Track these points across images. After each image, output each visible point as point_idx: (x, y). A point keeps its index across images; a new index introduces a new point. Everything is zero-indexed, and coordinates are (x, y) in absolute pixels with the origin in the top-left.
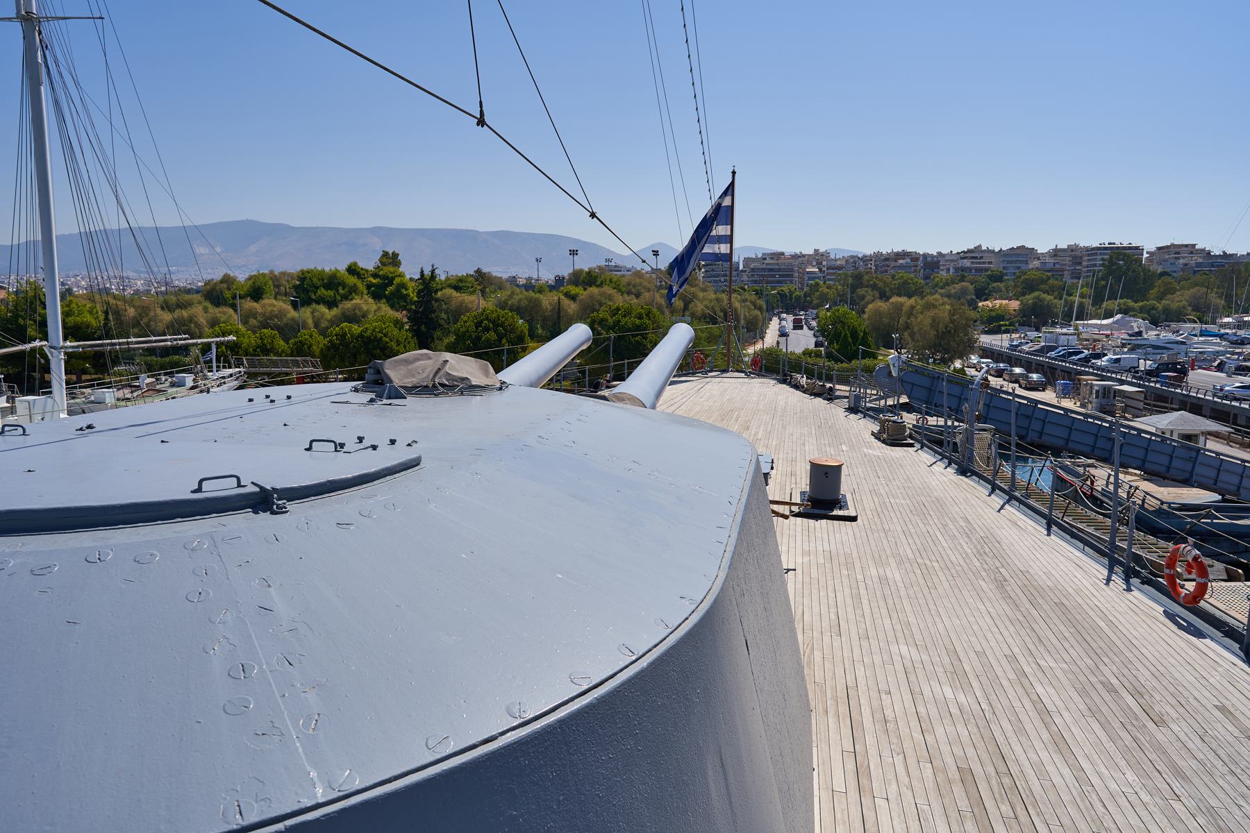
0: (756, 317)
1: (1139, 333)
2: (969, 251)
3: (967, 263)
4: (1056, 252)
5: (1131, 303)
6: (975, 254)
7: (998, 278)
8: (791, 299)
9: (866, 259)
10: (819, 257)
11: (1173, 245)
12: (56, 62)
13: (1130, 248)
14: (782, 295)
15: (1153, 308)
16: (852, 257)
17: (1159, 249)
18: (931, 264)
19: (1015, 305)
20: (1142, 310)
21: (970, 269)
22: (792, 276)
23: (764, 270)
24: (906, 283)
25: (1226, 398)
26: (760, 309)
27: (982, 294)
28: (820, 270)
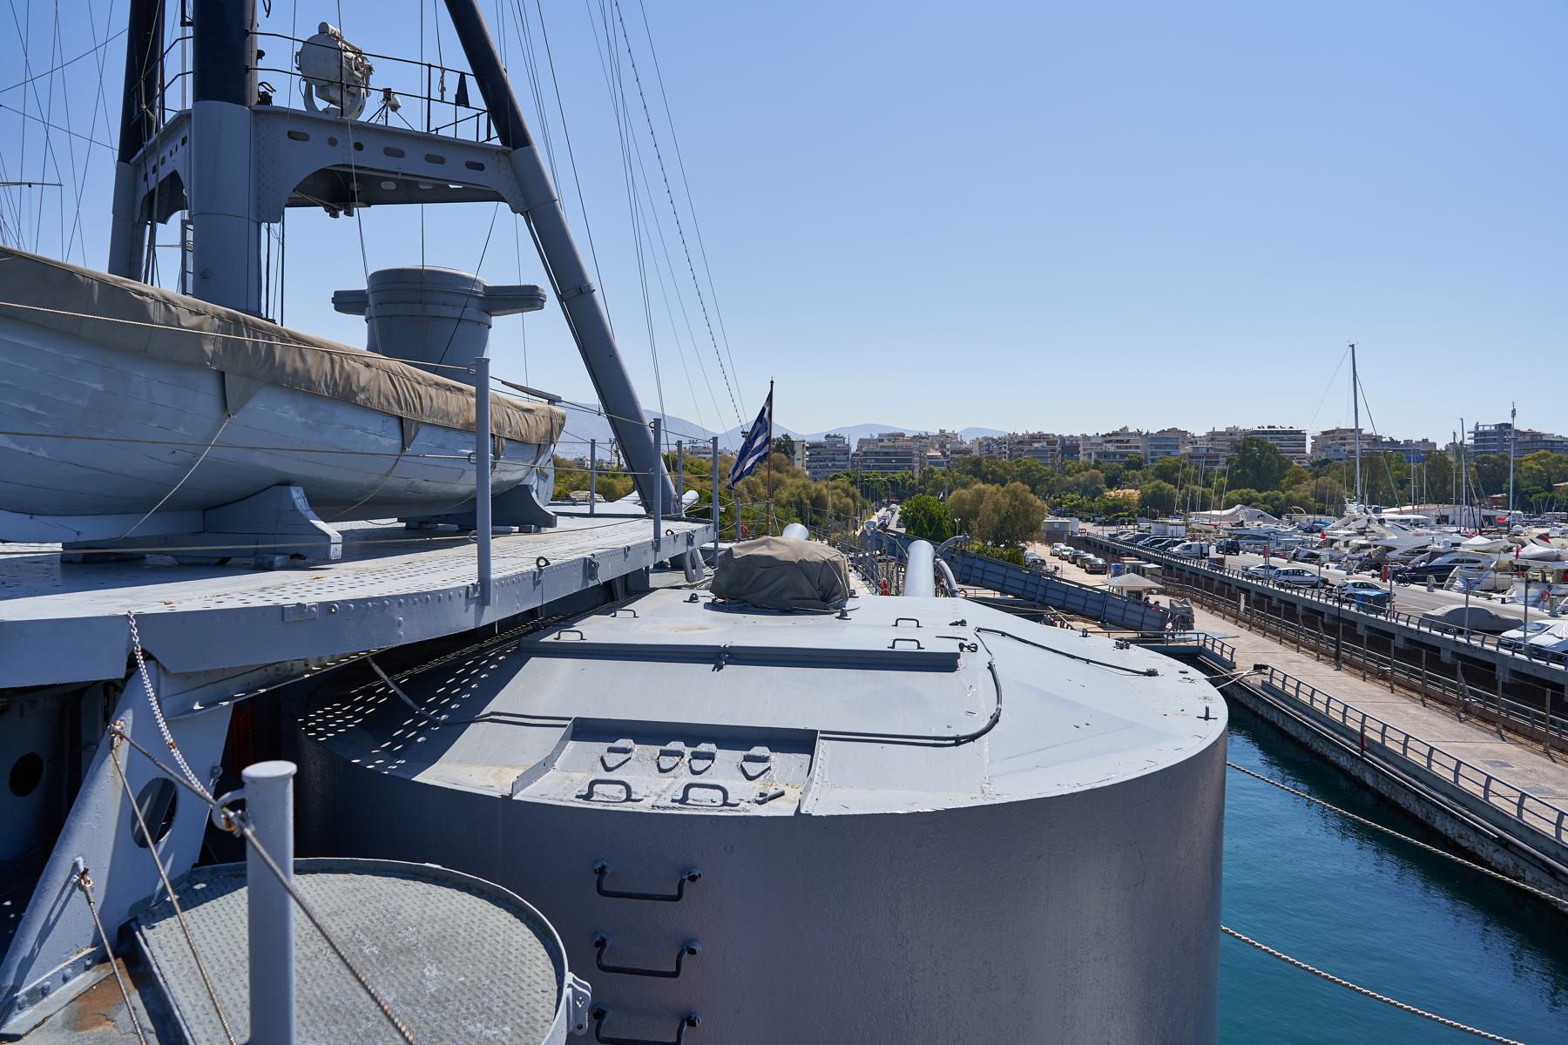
0: (847, 506)
1: (1241, 524)
2: (1115, 434)
3: (1111, 448)
4: (1213, 436)
5: (1254, 493)
7: (1138, 465)
8: (904, 487)
9: (999, 442)
10: (943, 439)
11: (1338, 430)
12: (1464, 805)
13: (1291, 432)
14: (894, 483)
15: (1277, 499)
16: (986, 439)
17: (1324, 433)
18: (1069, 447)
19: (1134, 494)
20: (1265, 500)
21: (1114, 455)
22: (910, 461)
23: (877, 453)
24: (1029, 470)
25: (1249, 577)
26: (853, 497)
27: (1113, 482)
28: (944, 454)
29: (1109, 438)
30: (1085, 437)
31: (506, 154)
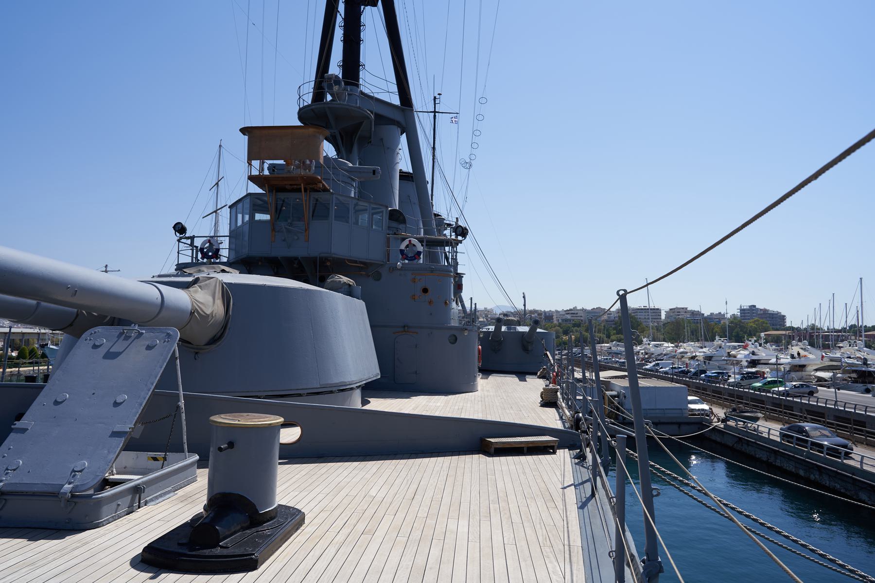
2: (571, 310)
3: (569, 317)
6: (572, 312)
21: (570, 320)
27: (566, 333)
29: (568, 312)
30: (557, 311)
31: (403, 110)
